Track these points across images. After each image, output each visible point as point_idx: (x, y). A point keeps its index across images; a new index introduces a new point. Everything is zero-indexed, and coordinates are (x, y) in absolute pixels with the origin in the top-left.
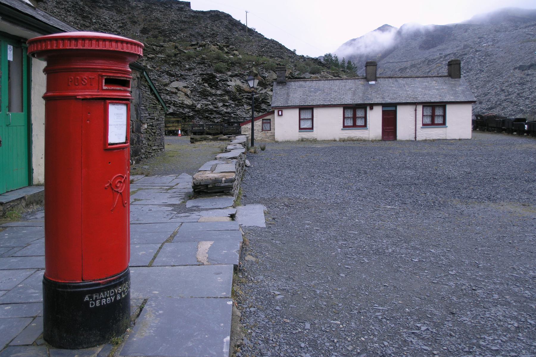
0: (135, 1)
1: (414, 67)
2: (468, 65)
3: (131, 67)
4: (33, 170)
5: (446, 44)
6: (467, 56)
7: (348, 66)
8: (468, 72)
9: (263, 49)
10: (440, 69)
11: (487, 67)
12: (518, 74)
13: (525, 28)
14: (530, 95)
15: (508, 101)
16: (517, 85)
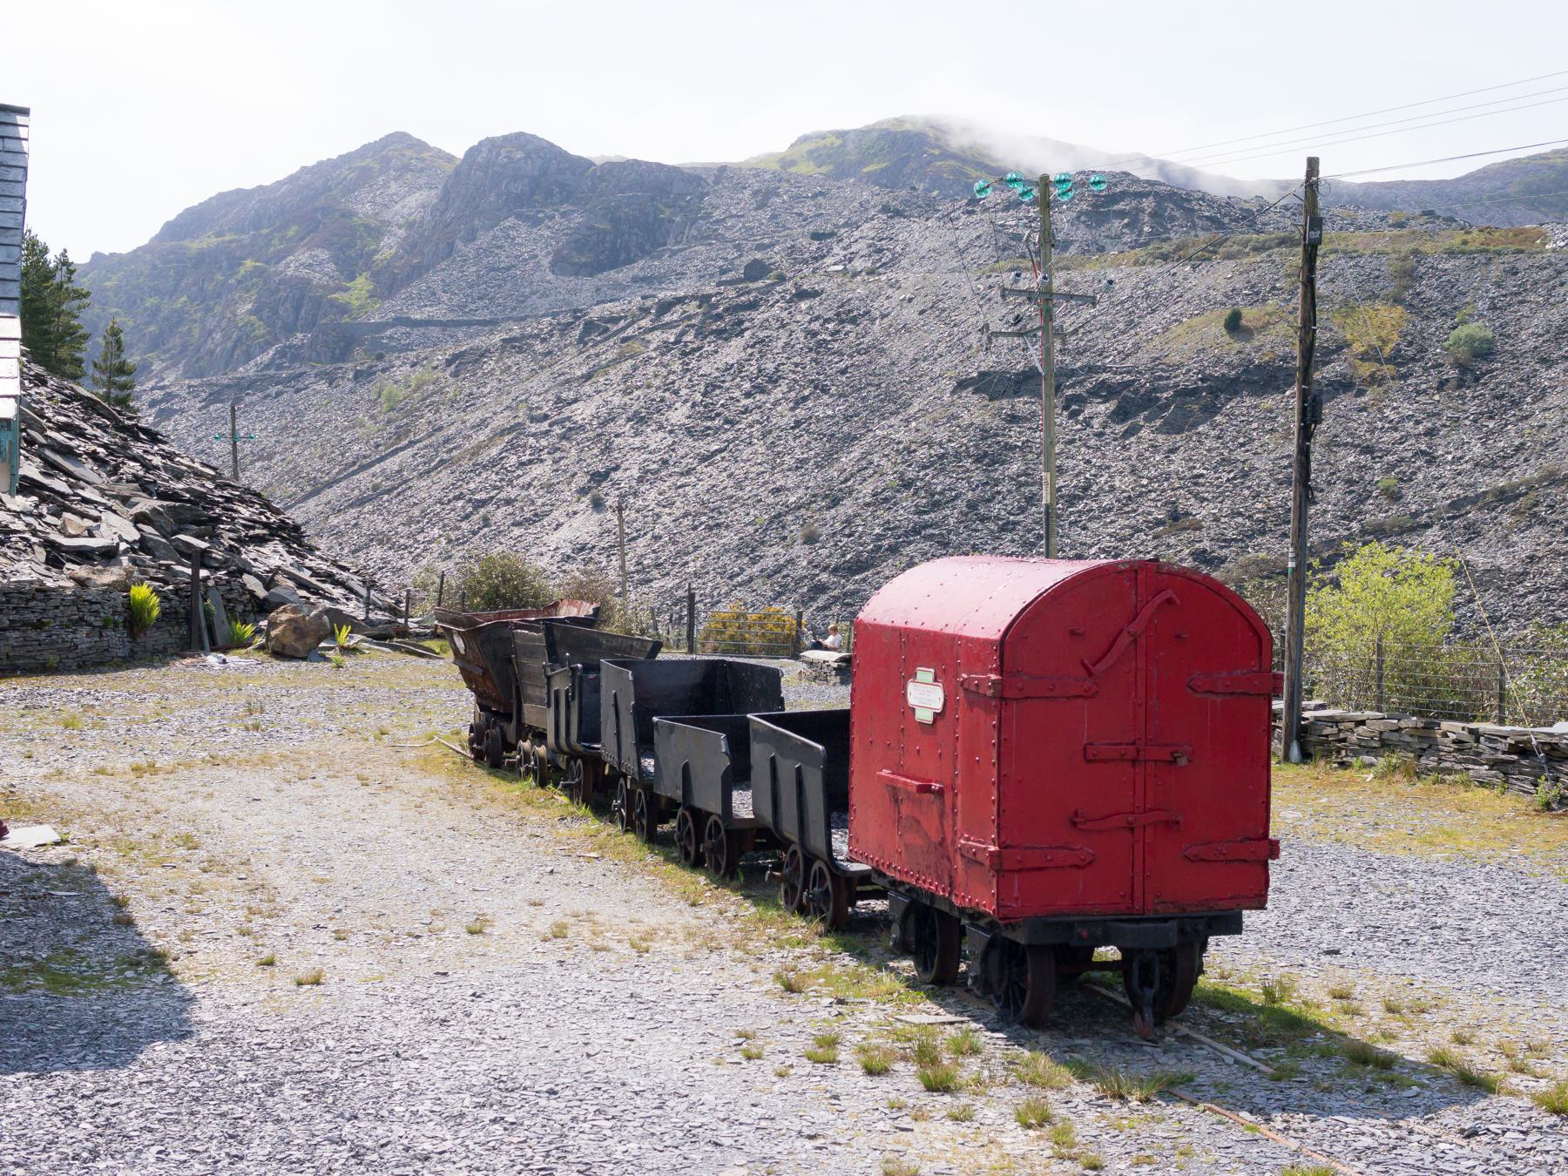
5: (674, 253)
6: (759, 316)
7: (352, 278)
8: (763, 391)
10: (635, 368)
11: (843, 372)
12: (976, 411)
13: (1006, 209)
14: (1022, 510)
16: (968, 463)
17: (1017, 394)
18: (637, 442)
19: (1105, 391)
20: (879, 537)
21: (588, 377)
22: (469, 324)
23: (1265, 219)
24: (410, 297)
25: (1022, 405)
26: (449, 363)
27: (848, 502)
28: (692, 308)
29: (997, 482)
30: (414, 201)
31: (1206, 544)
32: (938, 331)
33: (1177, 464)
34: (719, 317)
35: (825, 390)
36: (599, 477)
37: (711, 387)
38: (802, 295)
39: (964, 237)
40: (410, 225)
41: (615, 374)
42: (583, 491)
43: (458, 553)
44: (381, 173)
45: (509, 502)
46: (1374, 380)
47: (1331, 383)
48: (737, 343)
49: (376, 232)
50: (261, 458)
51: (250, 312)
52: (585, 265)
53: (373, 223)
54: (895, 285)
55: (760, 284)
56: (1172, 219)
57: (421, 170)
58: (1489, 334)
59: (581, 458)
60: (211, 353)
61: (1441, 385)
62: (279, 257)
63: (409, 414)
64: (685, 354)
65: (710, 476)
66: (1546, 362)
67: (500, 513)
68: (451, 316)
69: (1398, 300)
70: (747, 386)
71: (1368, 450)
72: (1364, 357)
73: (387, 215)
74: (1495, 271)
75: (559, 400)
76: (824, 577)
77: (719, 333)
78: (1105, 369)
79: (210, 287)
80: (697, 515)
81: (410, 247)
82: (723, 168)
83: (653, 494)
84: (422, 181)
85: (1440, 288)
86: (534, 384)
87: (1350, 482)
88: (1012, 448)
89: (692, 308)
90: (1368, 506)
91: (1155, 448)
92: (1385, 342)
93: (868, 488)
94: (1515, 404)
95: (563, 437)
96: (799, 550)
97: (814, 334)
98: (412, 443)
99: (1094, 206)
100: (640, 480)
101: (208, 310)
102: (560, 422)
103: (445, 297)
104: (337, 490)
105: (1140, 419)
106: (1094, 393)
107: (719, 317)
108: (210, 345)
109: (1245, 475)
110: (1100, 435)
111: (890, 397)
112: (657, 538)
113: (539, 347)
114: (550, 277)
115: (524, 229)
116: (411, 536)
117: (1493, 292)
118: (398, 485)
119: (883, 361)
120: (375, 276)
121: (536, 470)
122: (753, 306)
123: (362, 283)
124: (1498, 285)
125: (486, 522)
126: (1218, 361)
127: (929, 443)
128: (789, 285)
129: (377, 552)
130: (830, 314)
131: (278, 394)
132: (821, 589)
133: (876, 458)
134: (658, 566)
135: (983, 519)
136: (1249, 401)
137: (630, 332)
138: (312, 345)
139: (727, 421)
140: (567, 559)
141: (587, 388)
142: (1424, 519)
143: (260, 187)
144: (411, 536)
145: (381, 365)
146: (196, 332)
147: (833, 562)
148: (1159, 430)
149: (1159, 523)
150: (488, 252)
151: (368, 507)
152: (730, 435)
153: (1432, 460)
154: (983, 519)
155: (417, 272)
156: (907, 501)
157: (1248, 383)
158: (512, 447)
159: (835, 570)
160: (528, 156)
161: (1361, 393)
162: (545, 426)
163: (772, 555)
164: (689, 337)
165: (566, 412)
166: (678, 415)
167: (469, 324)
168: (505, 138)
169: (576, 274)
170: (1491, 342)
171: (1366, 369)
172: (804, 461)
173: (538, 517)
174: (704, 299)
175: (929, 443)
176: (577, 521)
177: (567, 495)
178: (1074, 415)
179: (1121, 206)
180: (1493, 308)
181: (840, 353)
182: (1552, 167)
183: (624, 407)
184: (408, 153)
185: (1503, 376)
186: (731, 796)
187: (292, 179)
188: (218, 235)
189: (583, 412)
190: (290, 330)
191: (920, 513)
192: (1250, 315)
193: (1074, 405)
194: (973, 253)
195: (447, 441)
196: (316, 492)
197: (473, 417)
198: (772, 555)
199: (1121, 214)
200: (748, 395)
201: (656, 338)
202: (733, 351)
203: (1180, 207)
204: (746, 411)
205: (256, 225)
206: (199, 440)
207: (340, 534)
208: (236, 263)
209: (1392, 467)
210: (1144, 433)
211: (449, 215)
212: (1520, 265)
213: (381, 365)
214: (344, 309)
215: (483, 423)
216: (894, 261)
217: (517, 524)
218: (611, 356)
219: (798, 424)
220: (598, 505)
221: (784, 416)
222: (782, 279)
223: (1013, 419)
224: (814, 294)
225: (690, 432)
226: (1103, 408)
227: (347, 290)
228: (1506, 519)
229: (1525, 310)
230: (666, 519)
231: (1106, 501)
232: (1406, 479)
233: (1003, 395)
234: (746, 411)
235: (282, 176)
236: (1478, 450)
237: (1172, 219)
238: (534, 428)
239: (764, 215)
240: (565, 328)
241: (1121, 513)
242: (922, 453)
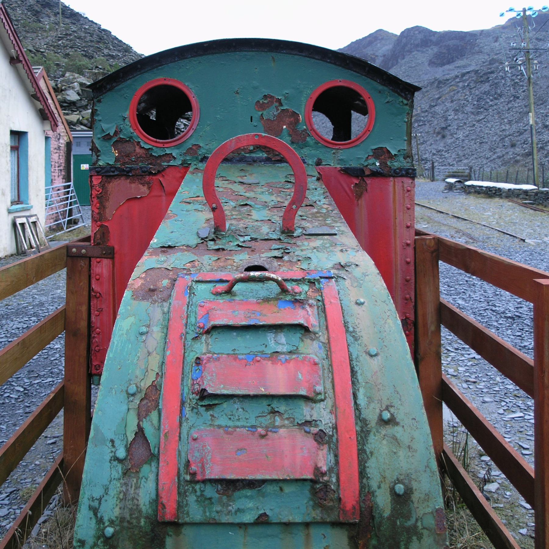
2: (496, 88)
5: (467, 58)
9: (60, 42)
10: (454, 94)
34: (481, 77)
76: (518, 158)
77: (482, 82)
82: (482, 31)
160: (420, 32)
162: (426, 114)
187: (349, 46)
225: (472, 113)
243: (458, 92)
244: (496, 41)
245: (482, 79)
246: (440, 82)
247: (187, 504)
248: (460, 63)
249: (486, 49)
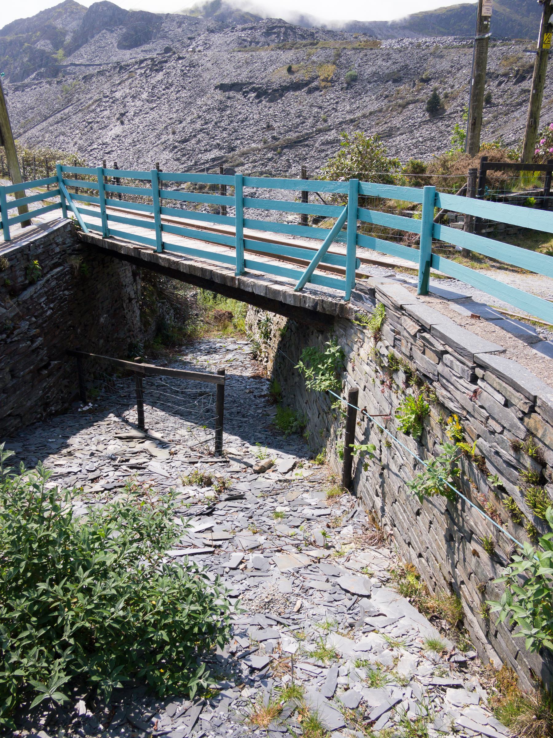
0: (549, 727)
1: (102, 75)
2: (168, 77)
3: (482, 308)
4: (281, 19)
5: (153, 42)
6: (168, 65)
7: (58, 50)
8: (168, 88)
10: (133, 81)
11: (190, 83)
12: (219, 95)
13: (242, 31)
14: (229, 124)
15: (204, 132)
16: (216, 111)
17: (231, 90)
18: (133, 104)
19: (254, 90)
20: (191, 132)
21: (119, 84)
22: (93, 65)
23: (317, 35)
24: (75, 56)
25: (231, 94)
26: (83, 79)
27: (184, 122)
28: (149, 62)
29: (223, 116)
30: (75, 23)
31: (275, 134)
32: (217, 70)
33: (271, 112)
34: (156, 65)
35: (185, 88)
36: (122, 115)
37: (154, 87)
38: (180, 58)
39: (229, 40)
40: (74, 32)
41: (127, 83)
42: (118, 119)
43: (84, 138)
44: (65, 13)
45: (98, 122)
46: (325, 87)
47: (313, 88)
48: (161, 73)
49: (64, 34)
50: (31, 109)
51: (27, 61)
52: (127, 46)
53: (63, 31)
54: (206, 55)
55: (168, 55)
56: (289, 35)
57: (76, 13)
58: (356, 74)
59: (118, 109)
60: (17, 74)
61: (342, 89)
62: (35, 42)
63: (71, 95)
64: (146, 77)
65: (154, 114)
66: (370, 83)
67: (95, 126)
68: (88, 63)
69: (334, 63)
70: (164, 87)
71: (320, 108)
72: (323, 80)
73: (67, 28)
74: (361, 55)
75: (112, 91)
76: (177, 144)
77: (156, 70)
78: (253, 83)
79: (15, 52)
80: (149, 126)
81: (75, 39)
82: (168, 14)
83: (137, 120)
84: (77, 17)
85: (346, 60)
86: (105, 86)
87: (315, 117)
88: (228, 107)
89: (149, 62)
90: (319, 124)
91: (266, 107)
92: (329, 76)
93: (190, 119)
94: (360, 95)
95: (113, 102)
96: (171, 136)
97: (183, 71)
98: (72, 104)
99: (267, 30)
100: (134, 116)
101: (15, 60)
102: (112, 98)
103: (86, 56)
104: (51, 119)
105: (263, 98)
106: (251, 90)
107: (156, 65)
108: (17, 72)
109: (288, 115)
110: (251, 103)
111: (202, 91)
112: (138, 133)
113: (108, 74)
114: (117, 50)
115: (108, 33)
116: (71, 133)
117: (360, 61)
118: (67, 118)
119: (201, 80)
120: (65, 49)
121: (105, 113)
122: (166, 62)
123: (61, 52)
124: (361, 59)
125: (92, 128)
126: (284, 81)
127: (206, 105)
128: (176, 55)
129: (62, 138)
130: (187, 65)
131: (35, 88)
132: (175, 147)
133: (192, 109)
134: (138, 141)
135: (219, 127)
136: (292, 93)
137: (132, 69)
138: (46, 72)
139: (158, 98)
140: (114, 139)
141: (119, 87)
142: (332, 127)
143: (28, 18)
144: (71, 133)
145: (64, 79)
146: (12, 67)
147: (179, 140)
148: (267, 102)
149: (264, 128)
150: (97, 41)
151: (60, 124)
152: (158, 102)
153: (336, 111)
154: (219, 127)
155: (78, 47)
156: (199, 123)
157: (292, 88)
158: (99, 106)
159: (179, 142)
160: (108, 9)
161: (321, 91)
162: (107, 99)
163: (164, 138)
164: (148, 72)
165: (114, 95)
166: (145, 96)
167: (93, 65)
168: (101, 3)
169: (125, 49)
170: (357, 76)
171: (323, 84)
172: (178, 110)
173: (106, 127)
174: (152, 59)
175: (206, 105)
176: (117, 128)
177: (114, 120)
178: (245, 97)
179: (275, 30)
180: (359, 66)
181: (189, 77)
182: (418, 17)
183: (130, 93)
184: (73, 7)
185: (358, 86)
186: (16, 223)
187: (37, 16)
188: (16, 34)
189: (118, 95)
190: (40, 67)
191: (202, 125)
192: (294, 67)
193: (245, 94)
194: (232, 45)
195: (81, 104)
196: (46, 120)
197: (89, 96)
198: (164, 138)
199: (275, 33)
200: (164, 90)
201: (139, 72)
202: (160, 76)
203: (292, 31)
204: (164, 94)
205: (28, 31)
206: (13, 103)
207: (52, 132)
208: (22, 45)
209: (326, 112)
210: (263, 102)
211: (86, 29)
212: (368, 53)
213: (64, 79)
214: (56, 60)
215: (91, 98)
216: (210, 47)
217: (100, 129)
218: (126, 77)
219: (177, 99)
220: (122, 123)
221: (173, 96)
222: (174, 53)
223: (229, 98)
224: (183, 58)
225: (148, 101)
226: (253, 95)
227: (56, 54)
228: (352, 127)
229: (367, 67)
230: (141, 127)
231: (251, 122)
232: (329, 116)
233: (227, 91)
234: (164, 94)
235: (34, 14)
236: (348, 108)
237: (289, 35)
238: (104, 100)
239: (180, 30)
240: (115, 68)
241: (255, 125)
242: (204, 108)
243: (136, 79)
244: (179, 27)
245: (157, 68)
246: (121, 68)
247: (220, 700)
248: (146, 47)
249: (171, 34)
